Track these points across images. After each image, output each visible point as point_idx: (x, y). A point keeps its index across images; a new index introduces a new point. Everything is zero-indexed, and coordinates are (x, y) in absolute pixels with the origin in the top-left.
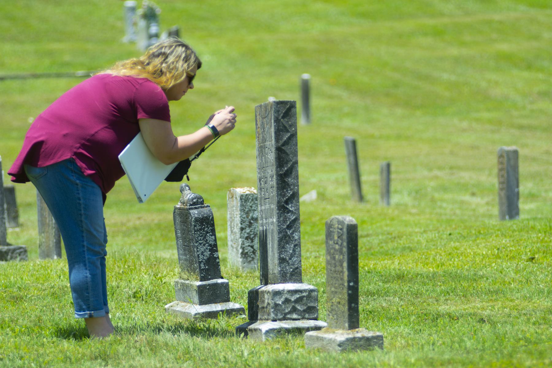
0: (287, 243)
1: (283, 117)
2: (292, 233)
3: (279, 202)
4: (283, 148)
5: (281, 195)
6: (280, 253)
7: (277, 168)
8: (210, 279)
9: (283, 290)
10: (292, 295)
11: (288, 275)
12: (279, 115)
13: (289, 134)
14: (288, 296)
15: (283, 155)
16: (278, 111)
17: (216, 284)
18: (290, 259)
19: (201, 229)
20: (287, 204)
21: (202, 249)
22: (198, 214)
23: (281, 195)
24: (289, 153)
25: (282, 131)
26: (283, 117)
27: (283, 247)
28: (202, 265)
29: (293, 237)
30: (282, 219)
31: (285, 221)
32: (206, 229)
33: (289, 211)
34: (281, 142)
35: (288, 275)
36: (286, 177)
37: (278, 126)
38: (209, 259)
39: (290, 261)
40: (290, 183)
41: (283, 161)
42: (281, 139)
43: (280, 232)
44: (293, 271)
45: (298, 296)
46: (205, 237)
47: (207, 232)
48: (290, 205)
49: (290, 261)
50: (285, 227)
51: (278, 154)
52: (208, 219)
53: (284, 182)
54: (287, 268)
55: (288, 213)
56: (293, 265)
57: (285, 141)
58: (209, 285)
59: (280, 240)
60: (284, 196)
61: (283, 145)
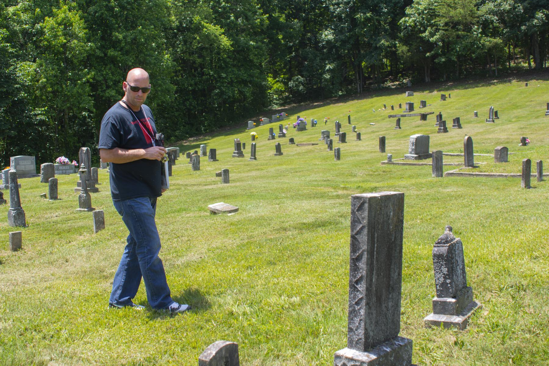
0: (355, 316)
1: (358, 210)
2: (359, 309)
3: (351, 281)
4: (356, 237)
5: (353, 275)
6: (349, 323)
7: (351, 252)
8: (443, 297)
9: (342, 356)
10: (349, 362)
11: (354, 343)
12: (355, 208)
13: (361, 226)
14: (346, 362)
15: (357, 243)
16: (355, 205)
17: (445, 302)
18: (356, 330)
19: (437, 262)
20: (357, 284)
21: (438, 276)
22: (438, 251)
23: (353, 275)
24: (360, 242)
25: (357, 222)
26: (358, 210)
27: (352, 319)
28: (438, 287)
29: (360, 313)
30: (352, 296)
31: (354, 298)
32: (441, 263)
33: (358, 291)
34: (355, 231)
35: (354, 343)
36: (358, 262)
37: (354, 218)
38: (442, 283)
39: (356, 332)
40: (360, 267)
41: (356, 247)
42: (356, 229)
43: (350, 306)
44: (358, 340)
45: (353, 364)
46: (440, 268)
47: (442, 265)
48: (359, 286)
49: (356, 332)
50: (354, 303)
51: (353, 241)
52: (443, 256)
53: (356, 265)
54: (354, 336)
55: (357, 292)
56: (358, 335)
57: (358, 231)
58: (440, 302)
59: (350, 313)
60: (355, 277)
61: (356, 234)
